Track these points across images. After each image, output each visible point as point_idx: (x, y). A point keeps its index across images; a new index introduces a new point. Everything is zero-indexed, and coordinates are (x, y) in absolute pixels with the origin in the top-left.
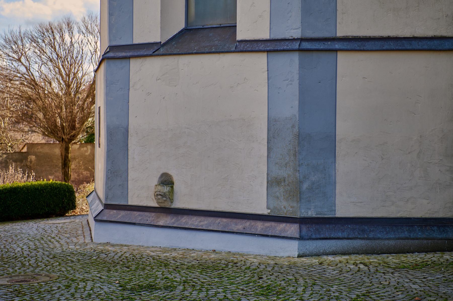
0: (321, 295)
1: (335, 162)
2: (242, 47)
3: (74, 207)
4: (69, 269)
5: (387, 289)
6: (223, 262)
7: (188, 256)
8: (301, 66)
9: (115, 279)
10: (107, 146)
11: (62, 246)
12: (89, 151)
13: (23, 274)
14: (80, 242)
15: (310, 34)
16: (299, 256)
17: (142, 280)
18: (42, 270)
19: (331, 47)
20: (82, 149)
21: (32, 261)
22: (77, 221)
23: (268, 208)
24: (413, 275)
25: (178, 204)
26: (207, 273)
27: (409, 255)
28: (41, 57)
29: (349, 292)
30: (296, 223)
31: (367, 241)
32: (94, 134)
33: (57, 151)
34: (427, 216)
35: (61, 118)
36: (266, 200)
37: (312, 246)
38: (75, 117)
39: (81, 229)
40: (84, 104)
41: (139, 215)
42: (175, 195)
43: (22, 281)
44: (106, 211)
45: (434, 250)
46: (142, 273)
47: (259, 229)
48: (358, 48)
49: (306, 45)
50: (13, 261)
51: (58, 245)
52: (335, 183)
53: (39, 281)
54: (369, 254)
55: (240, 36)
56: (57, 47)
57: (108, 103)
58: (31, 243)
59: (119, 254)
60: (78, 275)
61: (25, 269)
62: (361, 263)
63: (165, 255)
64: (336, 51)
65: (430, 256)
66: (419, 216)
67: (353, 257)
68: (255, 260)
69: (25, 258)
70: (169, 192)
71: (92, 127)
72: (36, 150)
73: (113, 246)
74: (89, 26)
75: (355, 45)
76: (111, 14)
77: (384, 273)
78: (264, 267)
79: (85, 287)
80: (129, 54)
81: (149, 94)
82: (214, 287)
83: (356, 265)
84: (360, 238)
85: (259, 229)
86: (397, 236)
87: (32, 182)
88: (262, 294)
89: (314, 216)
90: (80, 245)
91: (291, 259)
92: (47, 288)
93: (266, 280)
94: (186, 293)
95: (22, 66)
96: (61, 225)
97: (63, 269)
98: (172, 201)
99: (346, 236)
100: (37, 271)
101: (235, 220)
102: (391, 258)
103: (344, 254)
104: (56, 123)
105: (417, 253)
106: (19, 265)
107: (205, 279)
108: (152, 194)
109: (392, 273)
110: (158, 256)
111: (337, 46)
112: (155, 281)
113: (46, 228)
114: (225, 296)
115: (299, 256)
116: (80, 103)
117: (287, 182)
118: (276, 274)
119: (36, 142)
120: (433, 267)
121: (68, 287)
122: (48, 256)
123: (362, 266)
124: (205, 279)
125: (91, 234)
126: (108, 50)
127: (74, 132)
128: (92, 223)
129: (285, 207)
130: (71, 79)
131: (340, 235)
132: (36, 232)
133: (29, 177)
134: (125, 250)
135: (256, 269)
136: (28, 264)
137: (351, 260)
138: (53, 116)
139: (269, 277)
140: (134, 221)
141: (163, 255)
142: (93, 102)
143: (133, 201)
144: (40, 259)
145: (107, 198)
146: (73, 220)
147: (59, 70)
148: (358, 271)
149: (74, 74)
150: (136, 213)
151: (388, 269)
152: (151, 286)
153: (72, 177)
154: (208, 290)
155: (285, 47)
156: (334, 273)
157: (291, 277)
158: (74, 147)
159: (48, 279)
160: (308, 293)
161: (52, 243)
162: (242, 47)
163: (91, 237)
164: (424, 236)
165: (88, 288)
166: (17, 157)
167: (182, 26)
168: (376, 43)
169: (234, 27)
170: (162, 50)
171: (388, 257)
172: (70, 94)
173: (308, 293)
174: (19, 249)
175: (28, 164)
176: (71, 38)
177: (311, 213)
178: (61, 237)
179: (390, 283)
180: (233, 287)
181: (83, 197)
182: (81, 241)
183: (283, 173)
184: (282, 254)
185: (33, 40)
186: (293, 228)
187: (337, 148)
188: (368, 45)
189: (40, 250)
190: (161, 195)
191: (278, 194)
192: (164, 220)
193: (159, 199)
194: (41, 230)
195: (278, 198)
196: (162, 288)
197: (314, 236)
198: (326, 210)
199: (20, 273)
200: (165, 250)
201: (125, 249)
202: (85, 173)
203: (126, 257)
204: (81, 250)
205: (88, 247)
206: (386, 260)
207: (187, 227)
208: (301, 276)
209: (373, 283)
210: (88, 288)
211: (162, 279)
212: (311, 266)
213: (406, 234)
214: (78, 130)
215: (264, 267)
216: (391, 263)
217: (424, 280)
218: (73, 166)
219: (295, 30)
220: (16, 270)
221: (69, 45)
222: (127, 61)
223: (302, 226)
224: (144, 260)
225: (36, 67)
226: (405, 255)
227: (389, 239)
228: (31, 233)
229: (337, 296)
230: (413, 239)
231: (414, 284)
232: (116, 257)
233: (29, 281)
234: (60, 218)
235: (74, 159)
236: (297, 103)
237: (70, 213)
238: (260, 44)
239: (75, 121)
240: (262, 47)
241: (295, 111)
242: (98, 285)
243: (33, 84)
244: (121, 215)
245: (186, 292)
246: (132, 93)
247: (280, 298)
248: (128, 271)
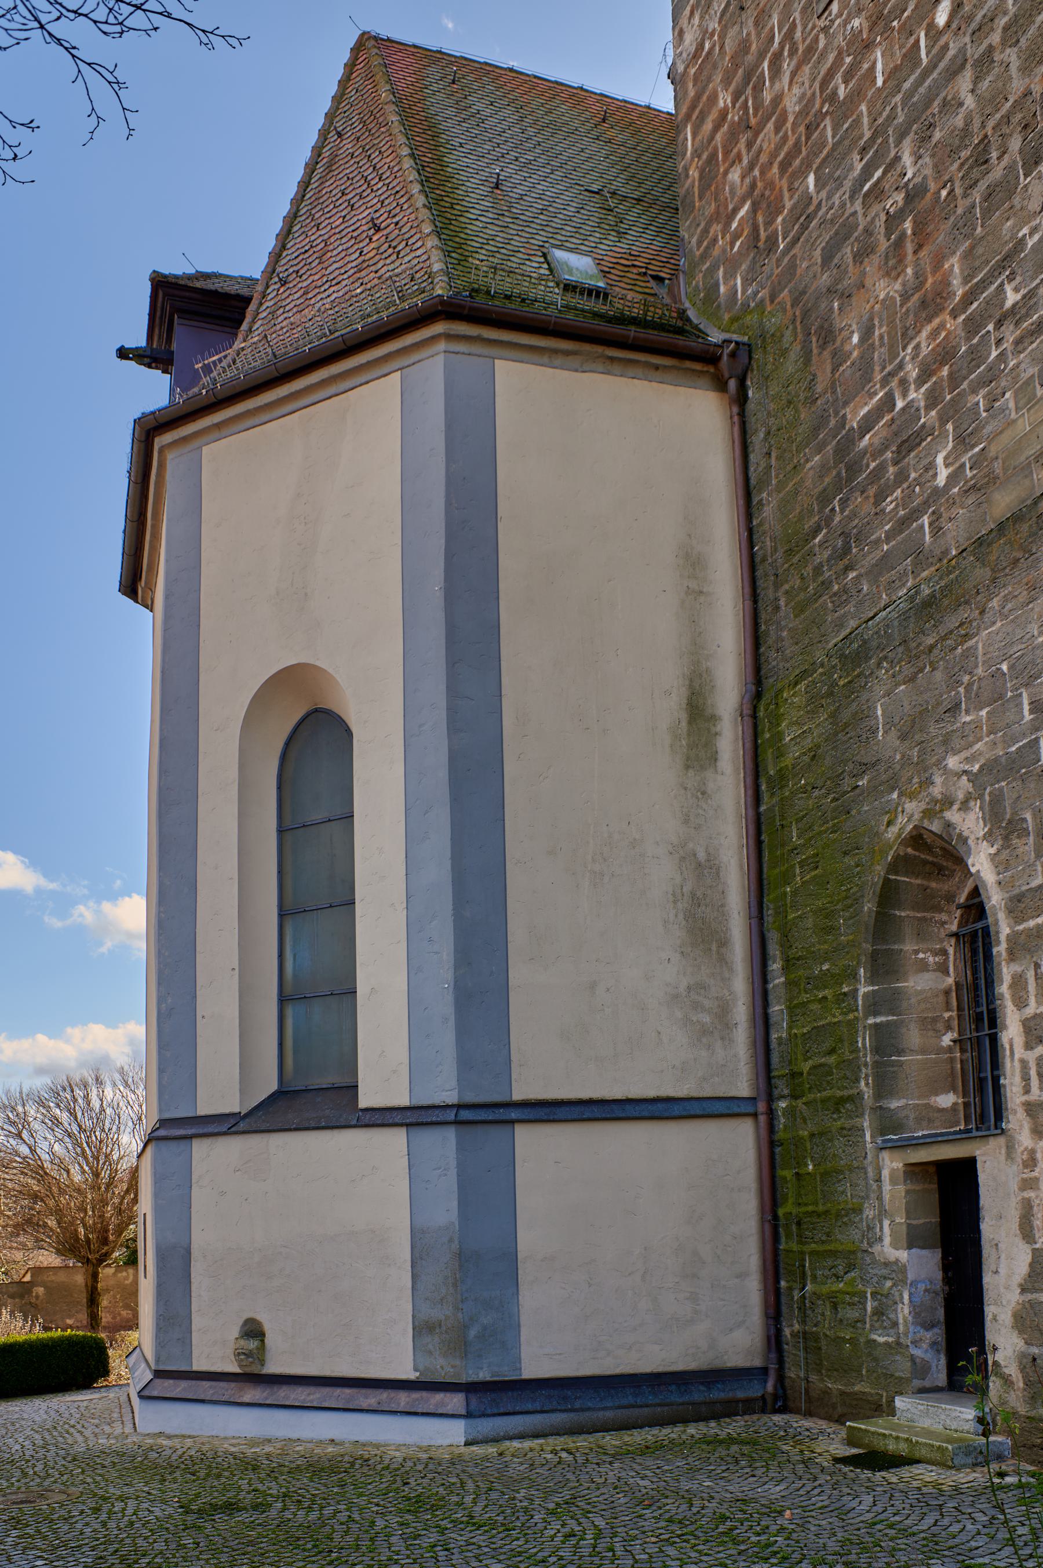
0: (501, 1506)
1: (518, 1293)
2: (367, 1118)
3: (105, 1372)
4: (98, 1478)
5: (602, 1490)
6: (346, 1458)
7: (290, 1451)
8: (461, 1148)
9: (172, 1494)
10: (158, 1276)
11: (86, 1439)
12: (131, 1278)
13: (23, 1489)
14: (115, 1433)
15: (471, 1098)
16: (467, 1444)
17: (216, 1494)
18: (55, 1482)
19: (504, 1118)
20: (120, 1275)
21: (39, 1467)
22: (112, 1395)
23: (416, 1370)
24: (641, 1464)
25: (273, 1368)
26: (320, 1479)
27: (635, 1432)
28: (53, 1130)
29: (545, 1499)
30: (460, 1391)
31: (572, 1415)
32: (136, 1251)
33: (80, 1279)
34: (661, 1369)
35: (85, 1226)
36: (412, 1358)
37: (487, 1426)
38: (108, 1225)
39: (117, 1410)
40: (121, 1203)
41: (211, 1387)
42: (267, 1353)
43: (22, 1502)
44: (158, 1381)
45: (672, 1422)
46: (216, 1483)
47: (402, 1404)
48: (545, 1117)
49: (465, 1115)
50: (8, 1467)
51: (80, 1439)
52: (519, 1326)
53: (49, 1502)
54: (574, 1433)
55: (363, 1103)
56: (79, 1115)
57: (157, 1209)
58: (37, 1436)
59: (179, 1452)
60: (112, 1490)
61: (27, 1480)
62: (562, 1450)
63: (253, 1450)
64: (512, 1122)
65: (666, 1431)
66: (648, 1369)
67: (551, 1440)
68: (398, 1454)
69: (28, 1461)
70: (257, 1348)
71: (134, 1240)
72: (45, 1278)
73: (169, 1437)
74: (130, 1080)
75: (541, 1113)
76: (161, 1071)
77: (597, 1464)
78: (412, 1464)
79: (124, 1509)
80: (190, 1132)
81: (223, 1193)
82: (332, 1502)
83: (556, 1454)
84: (560, 1411)
85: (402, 1404)
86: (617, 1404)
87: (39, 1334)
88: (409, 1511)
89: (488, 1379)
90: (116, 1438)
91: (454, 1449)
92: (63, 1513)
93: (416, 1486)
94: (288, 1515)
95: (24, 1145)
96: (85, 1404)
97: (89, 1480)
98: (262, 1362)
99: (539, 1409)
100: (46, 1484)
101: (364, 1391)
102: (608, 1438)
103: (536, 1436)
104: (77, 1236)
105: (647, 1429)
106: (18, 1474)
107: (316, 1488)
108: (230, 1351)
109: (611, 1463)
110: (243, 1453)
111: (514, 1115)
112: (238, 1495)
113: (62, 1410)
114: (350, 1517)
115: (467, 1444)
116: (116, 1201)
117: (444, 1328)
118: (430, 1476)
119: (45, 1264)
120: (671, 1450)
121: (97, 1510)
122: (64, 1458)
123: (564, 1455)
124: (316, 1488)
125: (133, 1418)
126: (158, 1125)
127: (106, 1248)
128: (135, 1400)
129: (442, 1367)
130: (101, 1162)
131: (529, 1407)
132: (45, 1417)
133: (33, 1325)
134: (189, 1445)
135: (399, 1469)
136: (31, 1472)
137: (548, 1445)
138: (72, 1223)
139: (419, 1482)
140: (202, 1397)
141: (250, 1452)
142: (135, 1201)
143: (200, 1364)
144: (51, 1464)
145: (158, 1360)
146: (105, 1394)
147: (83, 1150)
148: (559, 1463)
149: (106, 1157)
150: (206, 1384)
151: (604, 1458)
152: (231, 1504)
153: (104, 1320)
154: (322, 1508)
155: (434, 1119)
156: (521, 1468)
157: (453, 1480)
158: (106, 1272)
159: (64, 1497)
160: (481, 1504)
161: (71, 1435)
162: (367, 1118)
163: (134, 1424)
164: (657, 1401)
165: (130, 1511)
166: (15, 1289)
167: (274, 1086)
168: (573, 1108)
169: (353, 1088)
170: (242, 1126)
171: (604, 1438)
172: (99, 1188)
173: (481, 1504)
174: (18, 1447)
175: (33, 1300)
176: (101, 1100)
177: (484, 1375)
178: (86, 1425)
179: (606, 1479)
180: (362, 1501)
181: (120, 1356)
182: (118, 1430)
183: (437, 1313)
184: (439, 1442)
185: (41, 1103)
186: (455, 1400)
187: (520, 1272)
188: (561, 1113)
189: (50, 1447)
190: (244, 1354)
191: (430, 1346)
192: (251, 1394)
193: (242, 1360)
194: (52, 1413)
195: (430, 1353)
196: (249, 1507)
197: (489, 1411)
198: (506, 1368)
199: (19, 1488)
200: (253, 1442)
201: (189, 1442)
202: (124, 1313)
203: (191, 1457)
204: (117, 1445)
205: (129, 1440)
206: (602, 1442)
207: (287, 1403)
208: (471, 1476)
209: (581, 1481)
210: (130, 1511)
211: (248, 1493)
212: (486, 1458)
213: (631, 1400)
214: (112, 1245)
215: (412, 1464)
216: (609, 1447)
217: (658, 1471)
218: (105, 1302)
219: (449, 1093)
220: (13, 1484)
221: (97, 1111)
222: (187, 1141)
223: (470, 1396)
224: (219, 1460)
225: (45, 1145)
226: (629, 1432)
227: (605, 1409)
228: (37, 1419)
229: (526, 1508)
230: (641, 1406)
231: (642, 1479)
232: (174, 1457)
233: (34, 1502)
234: (84, 1392)
235: (108, 1290)
236: (455, 1204)
237: (101, 1383)
238: (395, 1113)
239: (107, 1231)
240: (398, 1119)
241: (453, 1216)
242: (146, 1505)
243: (40, 1173)
244: (180, 1388)
245: (287, 1513)
246: (198, 1195)
247: (437, 1516)
248: (194, 1481)
